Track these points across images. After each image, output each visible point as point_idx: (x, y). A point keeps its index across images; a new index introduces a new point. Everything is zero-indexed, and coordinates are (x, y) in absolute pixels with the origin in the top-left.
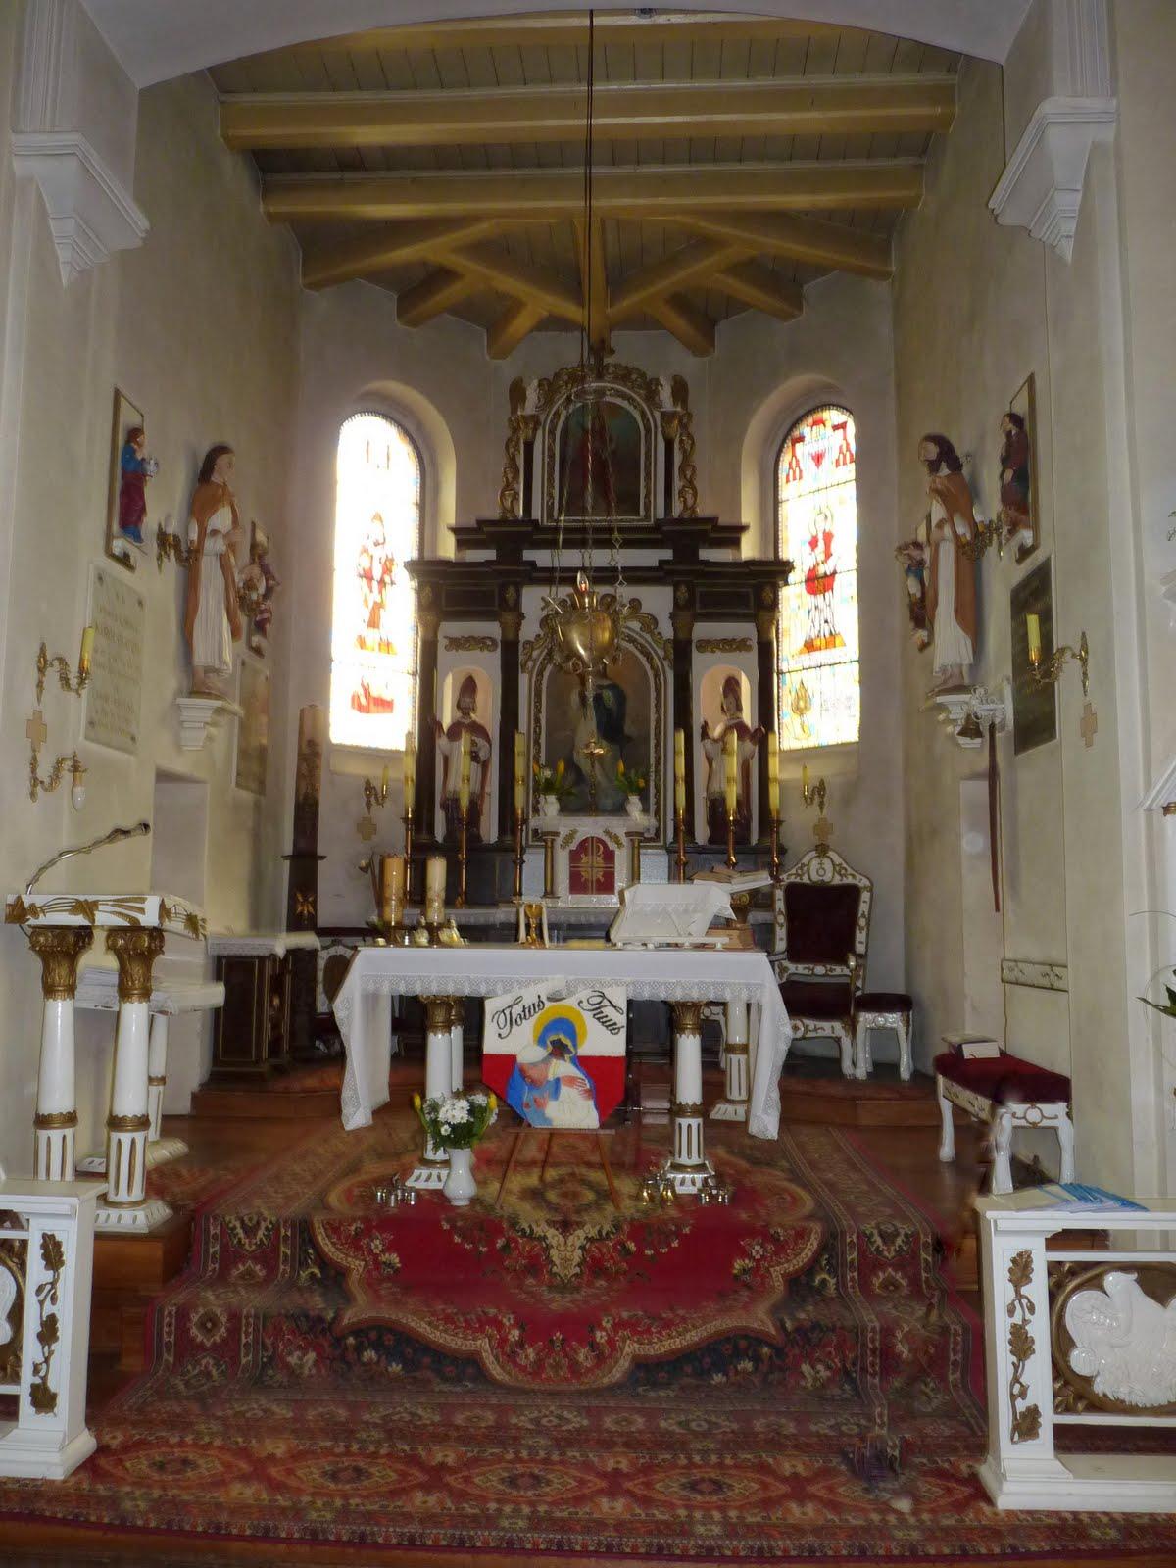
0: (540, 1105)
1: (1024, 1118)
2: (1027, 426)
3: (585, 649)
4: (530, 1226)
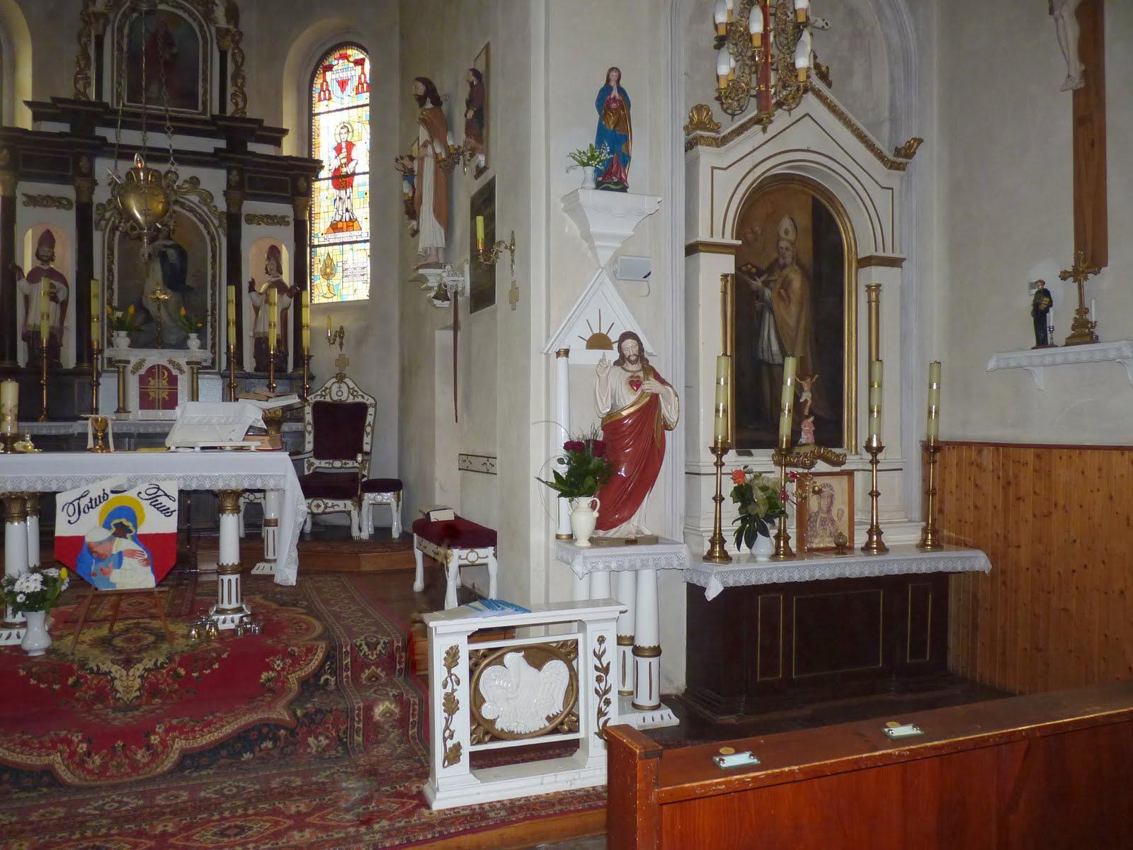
0: (106, 574)
1: (467, 559)
2: (484, 80)
3: (141, 214)
4: (97, 666)
